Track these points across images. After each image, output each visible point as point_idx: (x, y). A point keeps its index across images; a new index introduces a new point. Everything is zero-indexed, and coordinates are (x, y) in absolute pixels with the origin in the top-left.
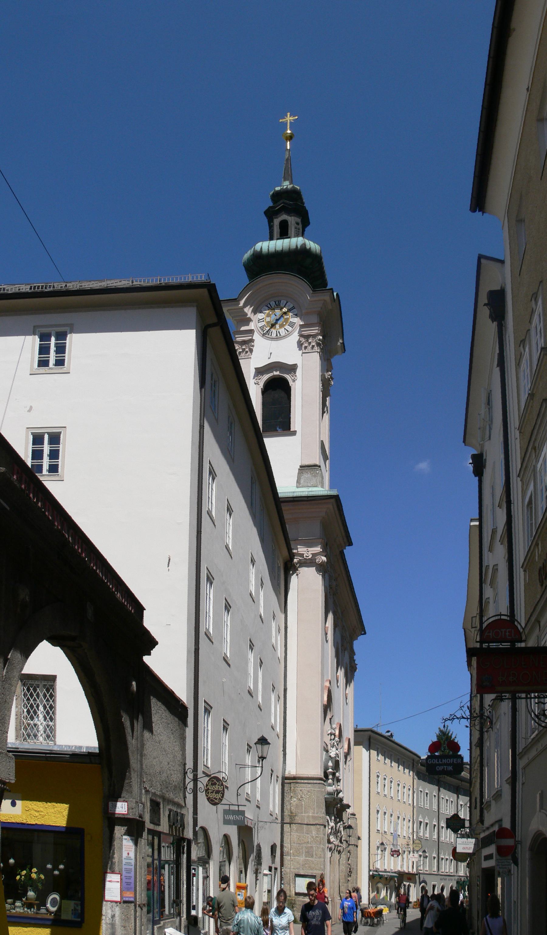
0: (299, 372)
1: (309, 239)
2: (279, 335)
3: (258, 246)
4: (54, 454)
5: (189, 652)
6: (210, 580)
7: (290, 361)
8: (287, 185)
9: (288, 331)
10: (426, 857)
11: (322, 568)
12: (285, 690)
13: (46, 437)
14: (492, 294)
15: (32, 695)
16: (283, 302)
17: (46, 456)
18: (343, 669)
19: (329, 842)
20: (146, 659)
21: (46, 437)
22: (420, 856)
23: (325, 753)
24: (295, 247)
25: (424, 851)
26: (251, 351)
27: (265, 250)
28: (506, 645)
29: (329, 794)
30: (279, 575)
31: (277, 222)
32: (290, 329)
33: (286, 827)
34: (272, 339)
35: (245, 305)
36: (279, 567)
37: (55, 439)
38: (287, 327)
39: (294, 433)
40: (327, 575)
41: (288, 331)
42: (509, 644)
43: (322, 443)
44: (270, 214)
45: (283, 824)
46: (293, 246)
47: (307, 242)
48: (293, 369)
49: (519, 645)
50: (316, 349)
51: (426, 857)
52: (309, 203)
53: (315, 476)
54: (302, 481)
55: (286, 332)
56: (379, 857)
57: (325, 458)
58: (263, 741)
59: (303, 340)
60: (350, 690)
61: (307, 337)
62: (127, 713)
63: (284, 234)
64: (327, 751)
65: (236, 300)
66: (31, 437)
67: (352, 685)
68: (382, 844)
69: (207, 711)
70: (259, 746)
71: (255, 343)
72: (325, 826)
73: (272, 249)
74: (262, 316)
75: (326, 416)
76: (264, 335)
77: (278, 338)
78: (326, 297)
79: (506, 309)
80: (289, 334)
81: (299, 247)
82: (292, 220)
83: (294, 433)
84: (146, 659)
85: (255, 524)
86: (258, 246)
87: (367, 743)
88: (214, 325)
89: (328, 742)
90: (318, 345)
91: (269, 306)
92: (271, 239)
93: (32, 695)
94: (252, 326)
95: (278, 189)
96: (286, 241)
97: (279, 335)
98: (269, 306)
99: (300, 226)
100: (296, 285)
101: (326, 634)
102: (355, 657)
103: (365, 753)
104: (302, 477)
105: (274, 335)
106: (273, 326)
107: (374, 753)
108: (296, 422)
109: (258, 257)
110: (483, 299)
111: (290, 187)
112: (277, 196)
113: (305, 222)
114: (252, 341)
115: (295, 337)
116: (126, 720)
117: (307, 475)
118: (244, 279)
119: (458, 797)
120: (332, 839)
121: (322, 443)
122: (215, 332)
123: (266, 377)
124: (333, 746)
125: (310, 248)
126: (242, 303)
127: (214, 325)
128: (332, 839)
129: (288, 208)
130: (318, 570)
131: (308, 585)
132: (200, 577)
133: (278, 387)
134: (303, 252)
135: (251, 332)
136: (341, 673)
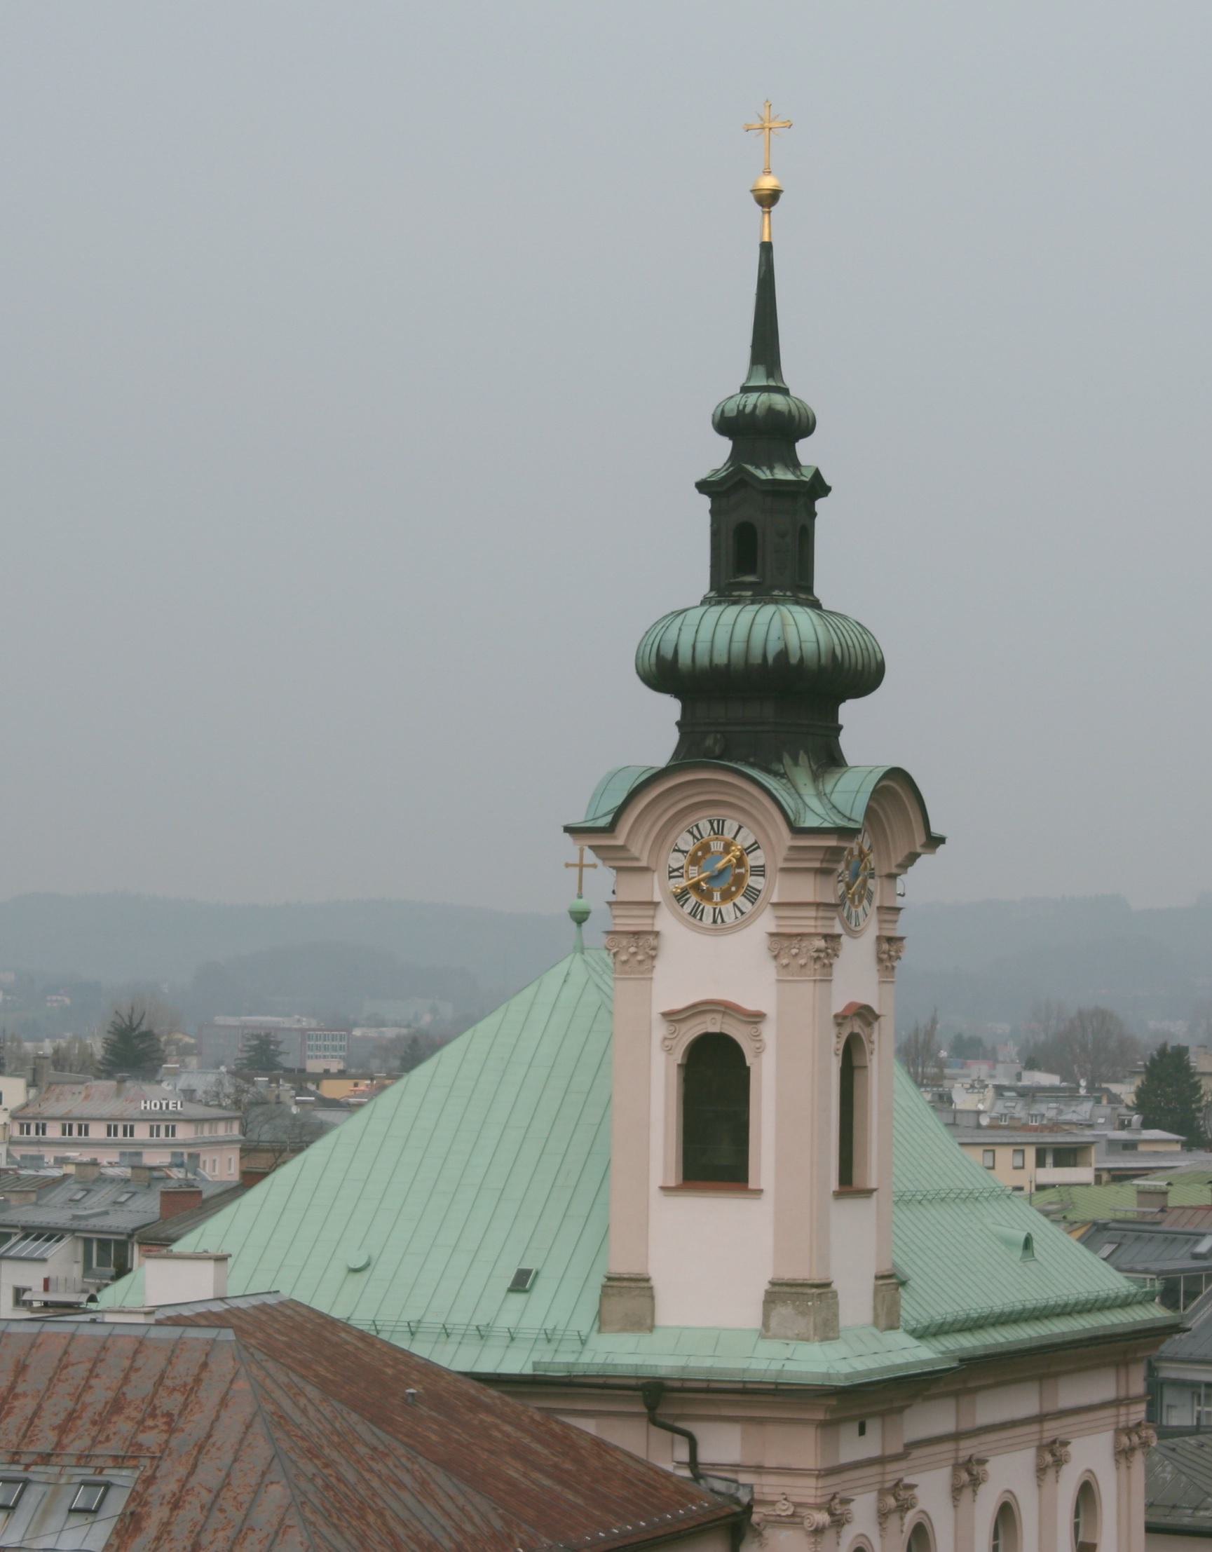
2: (719, 920)
9: (742, 913)
17: (94, 1156)
18: (803, 758)
24: (759, 661)
38: (740, 900)
41: (742, 913)
48: (756, 1018)
53: (803, 1314)
54: (773, 1323)
55: (738, 914)
74: (678, 860)
79: (682, 1091)
81: (770, 659)
91: (696, 832)
97: (719, 920)
98: (696, 832)
104: (774, 1313)
117: (784, 1311)
119: (711, 660)
125: (802, 659)
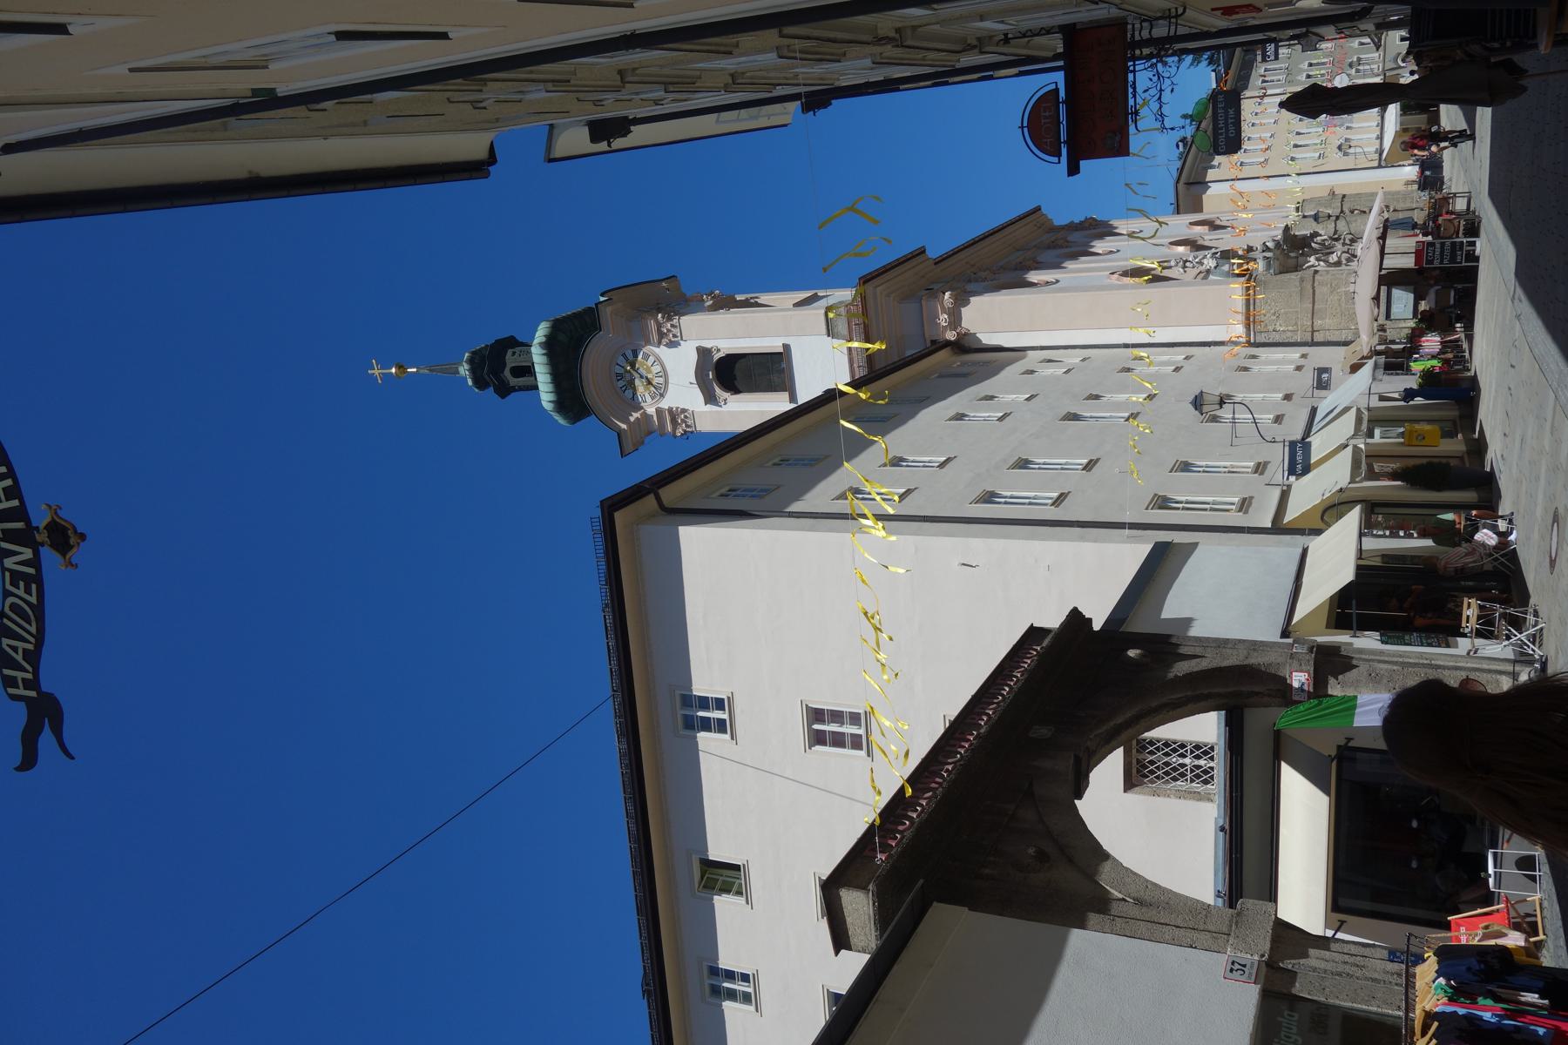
0: (707, 344)
1: (533, 338)
3: (548, 406)
4: (837, 716)
5: (1082, 539)
6: (989, 497)
7: (694, 357)
8: (464, 370)
10: (1359, 59)
11: (962, 300)
12: (1126, 346)
13: (816, 727)
14: (595, 138)
15: (1152, 772)
16: (618, 370)
19: (1338, 264)
20: (1097, 626)
21: (816, 727)
22: (1358, 71)
23: (1211, 277)
25: (1351, 65)
26: (684, 411)
27: (551, 397)
28: (1062, 109)
29: (1268, 266)
30: (975, 363)
31: (513, 381)
32: (651, 359)
33: (1319, 337)
34: (666, 382)
35: (626, 421)
36: (963, 364)
37: (816, 715)
38: (650, 362)
39: (786, 347)
40: (970, 287)
42: (1061, 63)
43: (798, 304)
44: (504, 391)
45: (1313, 344)
46: (544, 359)
47: (536, 341)
48: (704, 353)
49: (1062, 94)
50: (675, 322)
51: (1359, 59)
52: (485, 340)
56: (1359, 150)
57: (814, 299)
58: (1198, 403)
59: (665, 341)
60: (1123, 226)
61: (661, 335)
62: (1170, 666)
63: (528, 371)
64: (1208, 272)
65: (620, 433)
66: (818, 748)
67: (1114, 223)
68: (1340, 148)
69: (1163, 503)
70: (1205, 408)
71: (674, 405)
72: (1316, 272)
73: (550, 387)
75: (764, 298)
76: (662, 395)
77: (664, 373)
78: (607, 313)
80: (658, 360)
82: (512, 360)
83: (786, 347)
84: (1097, 626)
85: (912, 415)
86: (548, 406)
87: (1194, 189)
88: (658, 498)
89: (1196, 271)
90: (670, 319)
92: (536, 388)
93: (1152, 772)
94: (651, 411)
95: (470, 382)
96: (538, 368)
99: (517, 350)
100: (595, 359)
101: (1047, 283)
102: (1077, 221)
103: (1214, 189)
105: (661, 380)
106: (649, 382)
107: (1211, 175)
108: (772, 344)
109: (561, 405)
110: (603, 146)
111: (466, 366)
112: (480, 383)
113: (511, 343)
114: (670, 410)
115: (662, 351)
116: (1181, 668)
118: (591, 420)
120: (1333, 258)
121: (798, 304)
122: (670, 494)
123: (718, 391)
124: (1201, 263)
126: (624, 426)
127: (658, 498)
128: (1333, 258)
129: (497, 367)
130: (966, 303)
131: (990, 317)
132: (988, 515)
133: (728, 373)
134: (550, 345)
135: (659, 411)
136: (1099, 246)
